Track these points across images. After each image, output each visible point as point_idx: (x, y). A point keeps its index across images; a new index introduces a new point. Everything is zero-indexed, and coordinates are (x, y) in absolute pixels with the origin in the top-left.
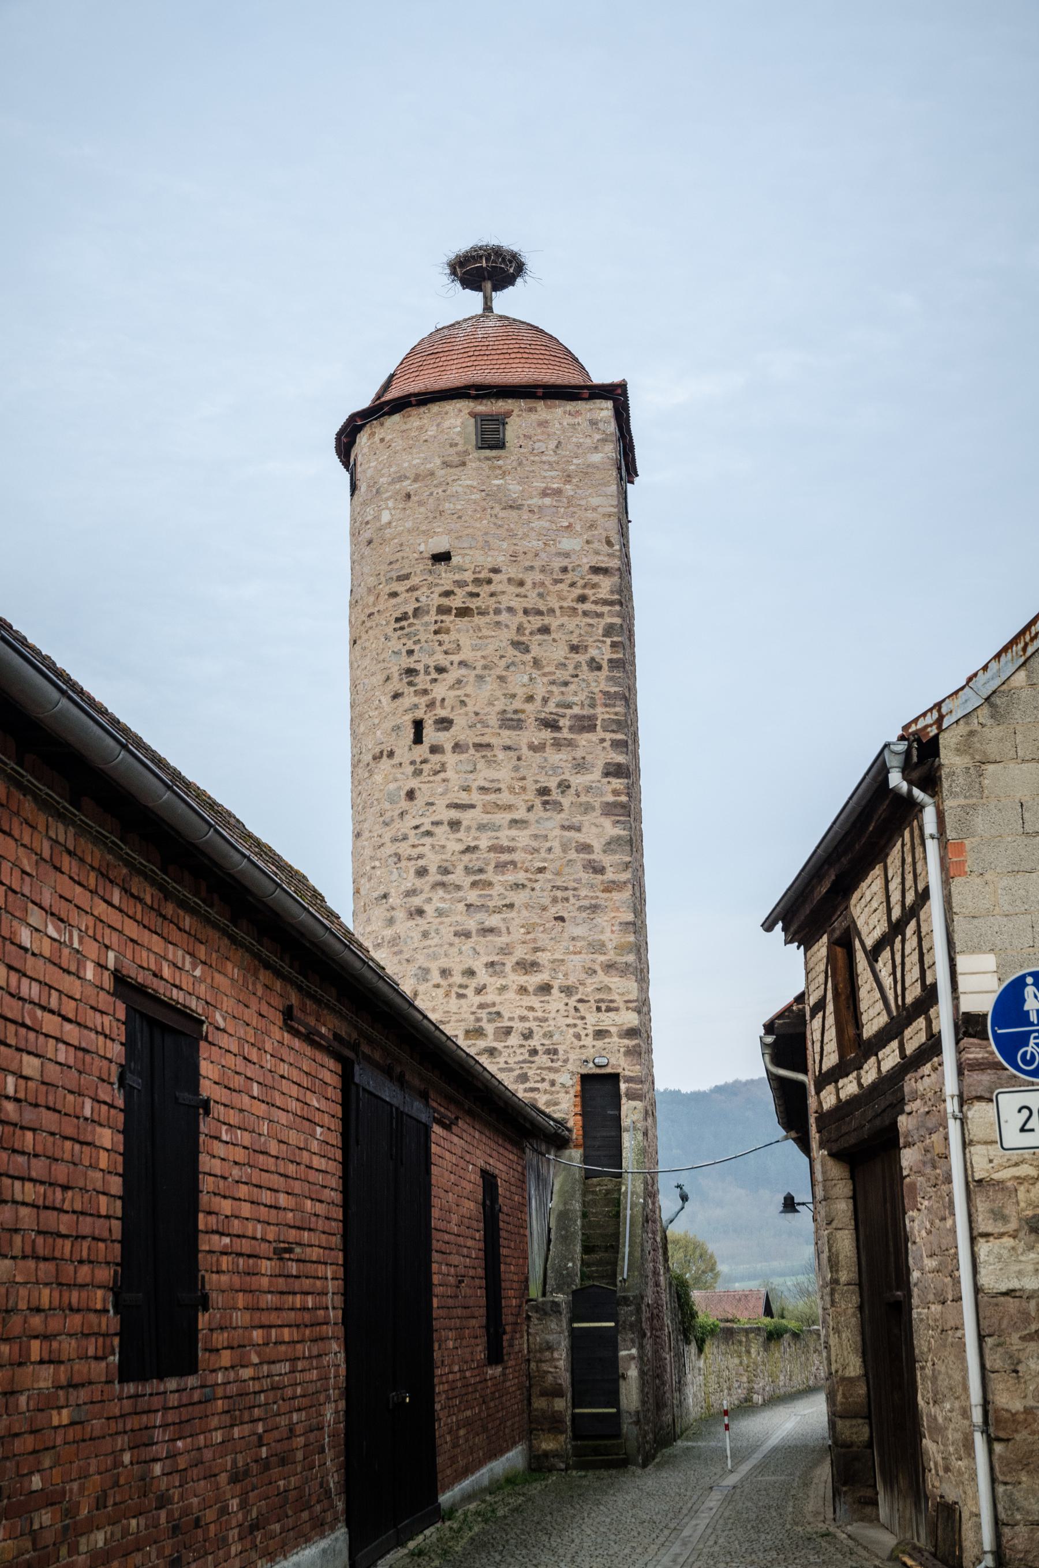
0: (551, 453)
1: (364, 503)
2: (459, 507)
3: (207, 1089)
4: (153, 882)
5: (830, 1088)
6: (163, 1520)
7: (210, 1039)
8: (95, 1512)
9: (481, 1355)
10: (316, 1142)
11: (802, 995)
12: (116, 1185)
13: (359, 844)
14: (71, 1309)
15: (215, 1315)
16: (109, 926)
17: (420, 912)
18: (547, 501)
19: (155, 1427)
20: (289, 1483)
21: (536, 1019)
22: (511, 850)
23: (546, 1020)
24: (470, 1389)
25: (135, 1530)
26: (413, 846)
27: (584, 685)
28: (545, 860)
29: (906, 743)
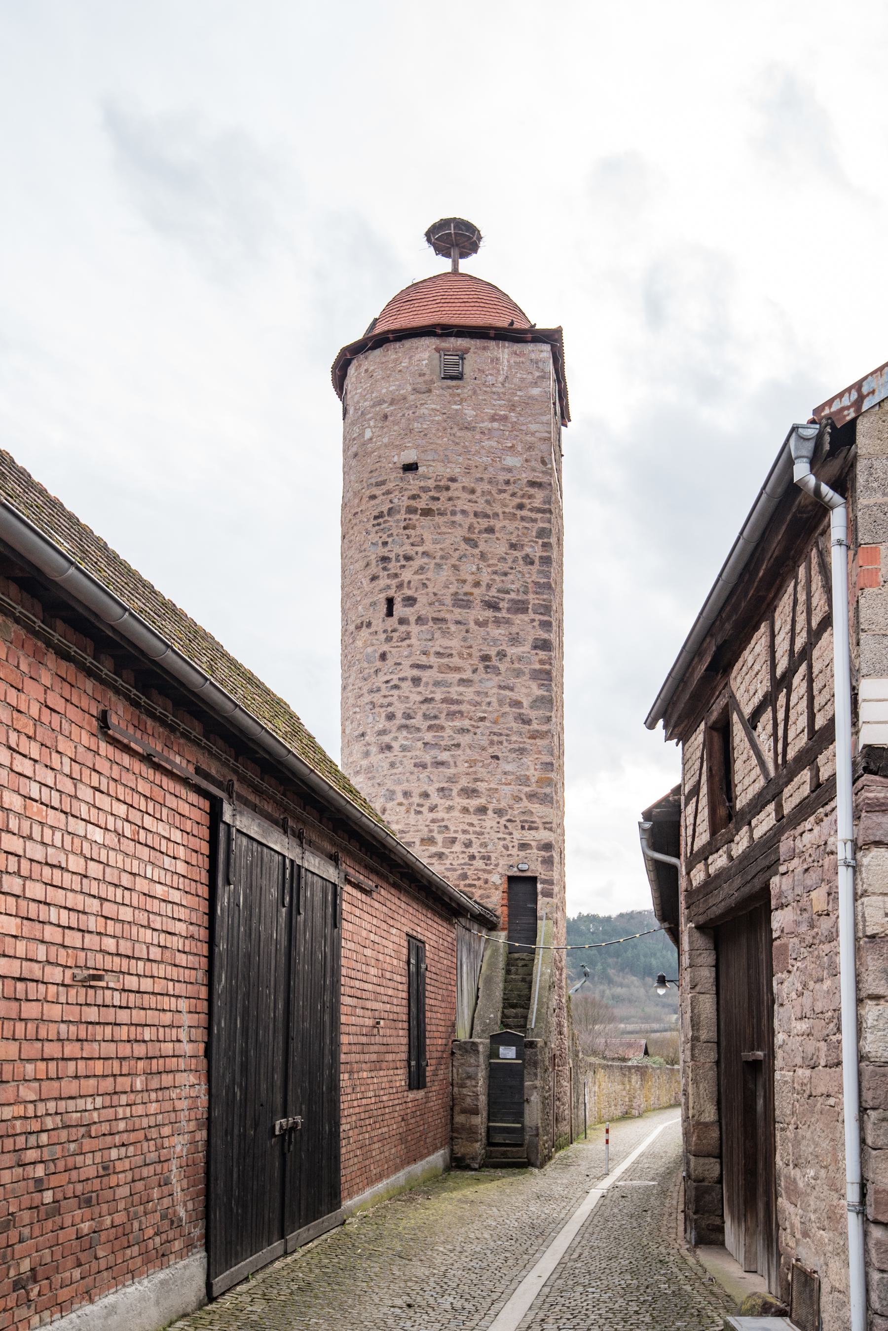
0: (500, 385)
1: (353, 424)
2: (425, 426)
5: (701, 866)
9: (400, 1078)
13: (345, 695)
17: (389, 747)
18: (495, 425)
21: (475, 833)
22: (458, 702)
23: (483, 834)
26: (385, 697)
27: (520, 576)
28: (485, 712)
29: (818, 426)
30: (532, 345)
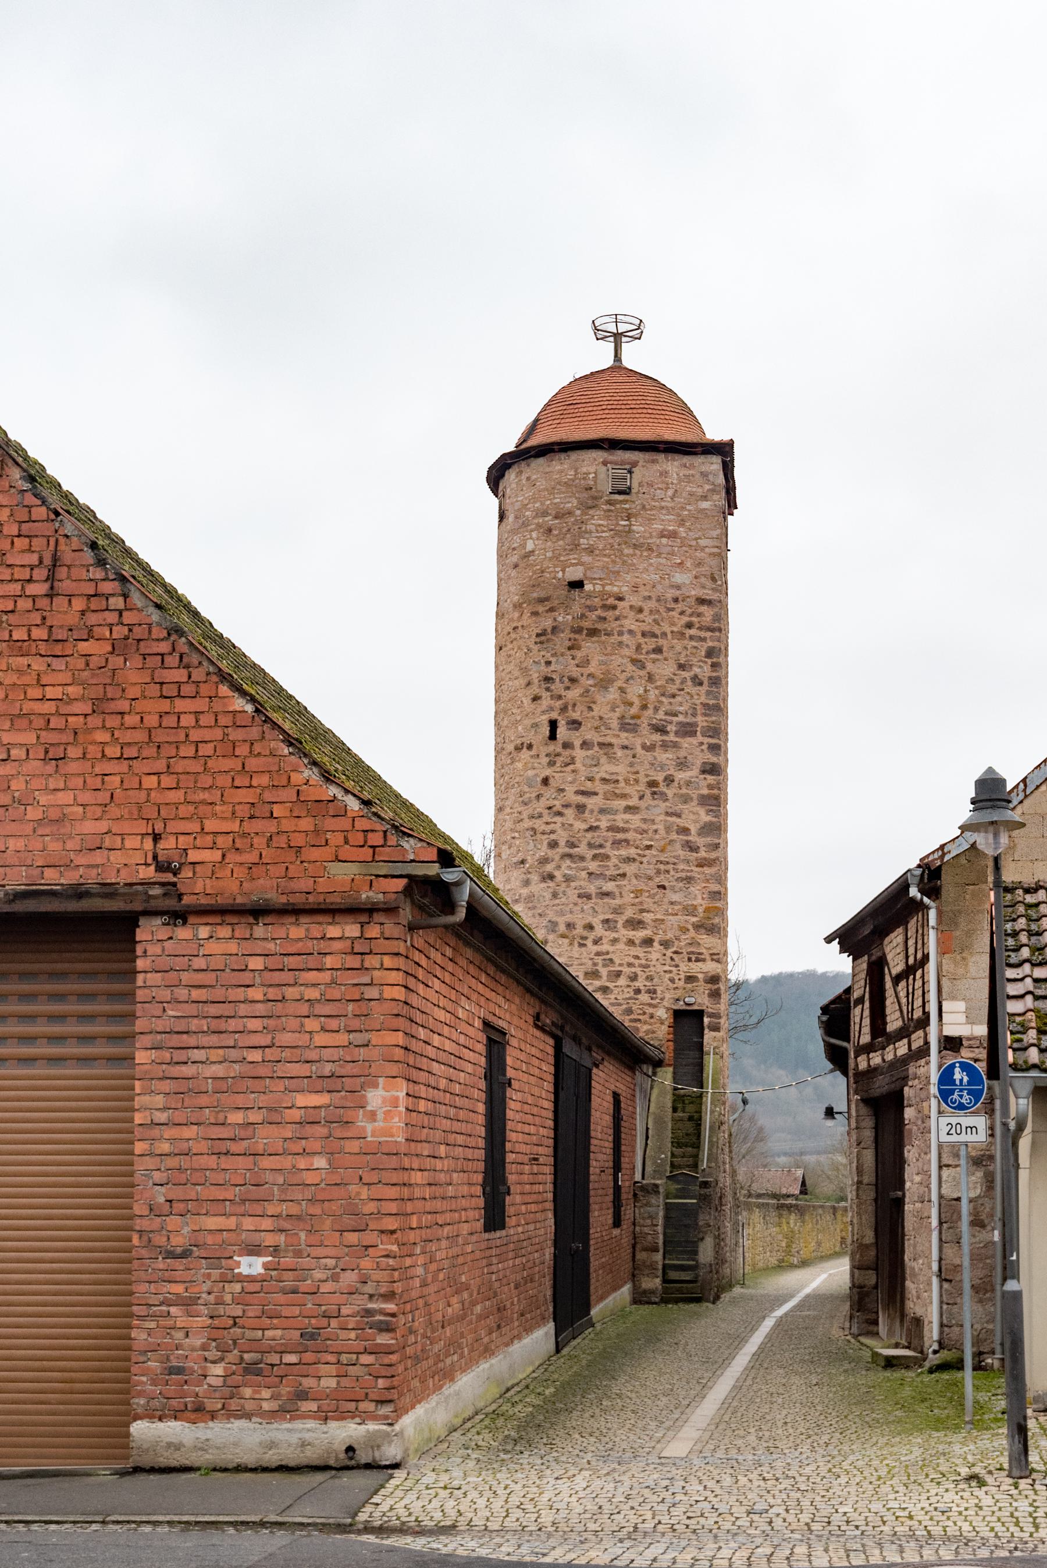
3: (510, 1073)
9: (610, 1221)
13: (500, 817)
17: (551, 877)
18: (664, 541)
22: (624, 830)
26: (547, 823)
27: (688, 698)
30: (702, 457)
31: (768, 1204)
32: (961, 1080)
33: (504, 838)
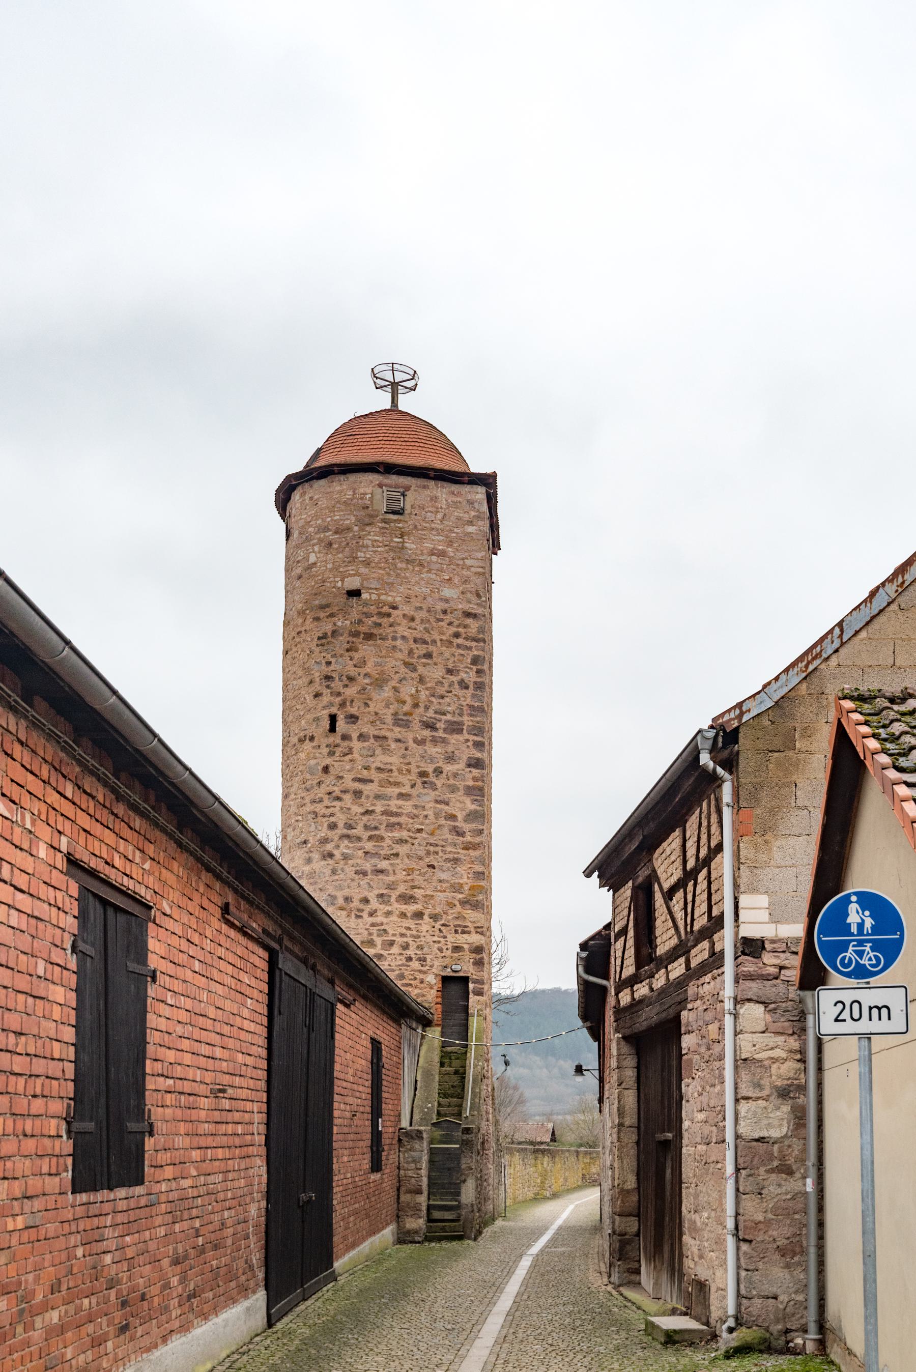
1: (298, 547)
3: (153, 962)
4: (106, 784)
5: (627, 991)
6: (113, 1297)
7: (157, 922)
8: (50, 1296)
9: (366, 1164)
10: (247, 1010)
11: (610, 924)
12: (69, 1034)
13: (286, 803)
14: (25, 1135)
15: (159, 1140)
16: (62, 815)
17: (331, 855)
18: (434, 558)
19: (106, 1227)
20: (221, 1262)
22: (397, 815)
24: (358, 1189)
25: (88, 1307)
26: (327, 807)
27: (455, 699)
28: (422, 824)
30: (469, 486)
31: (526, 1149)
32: (861, 926)
33: (289, 822)
